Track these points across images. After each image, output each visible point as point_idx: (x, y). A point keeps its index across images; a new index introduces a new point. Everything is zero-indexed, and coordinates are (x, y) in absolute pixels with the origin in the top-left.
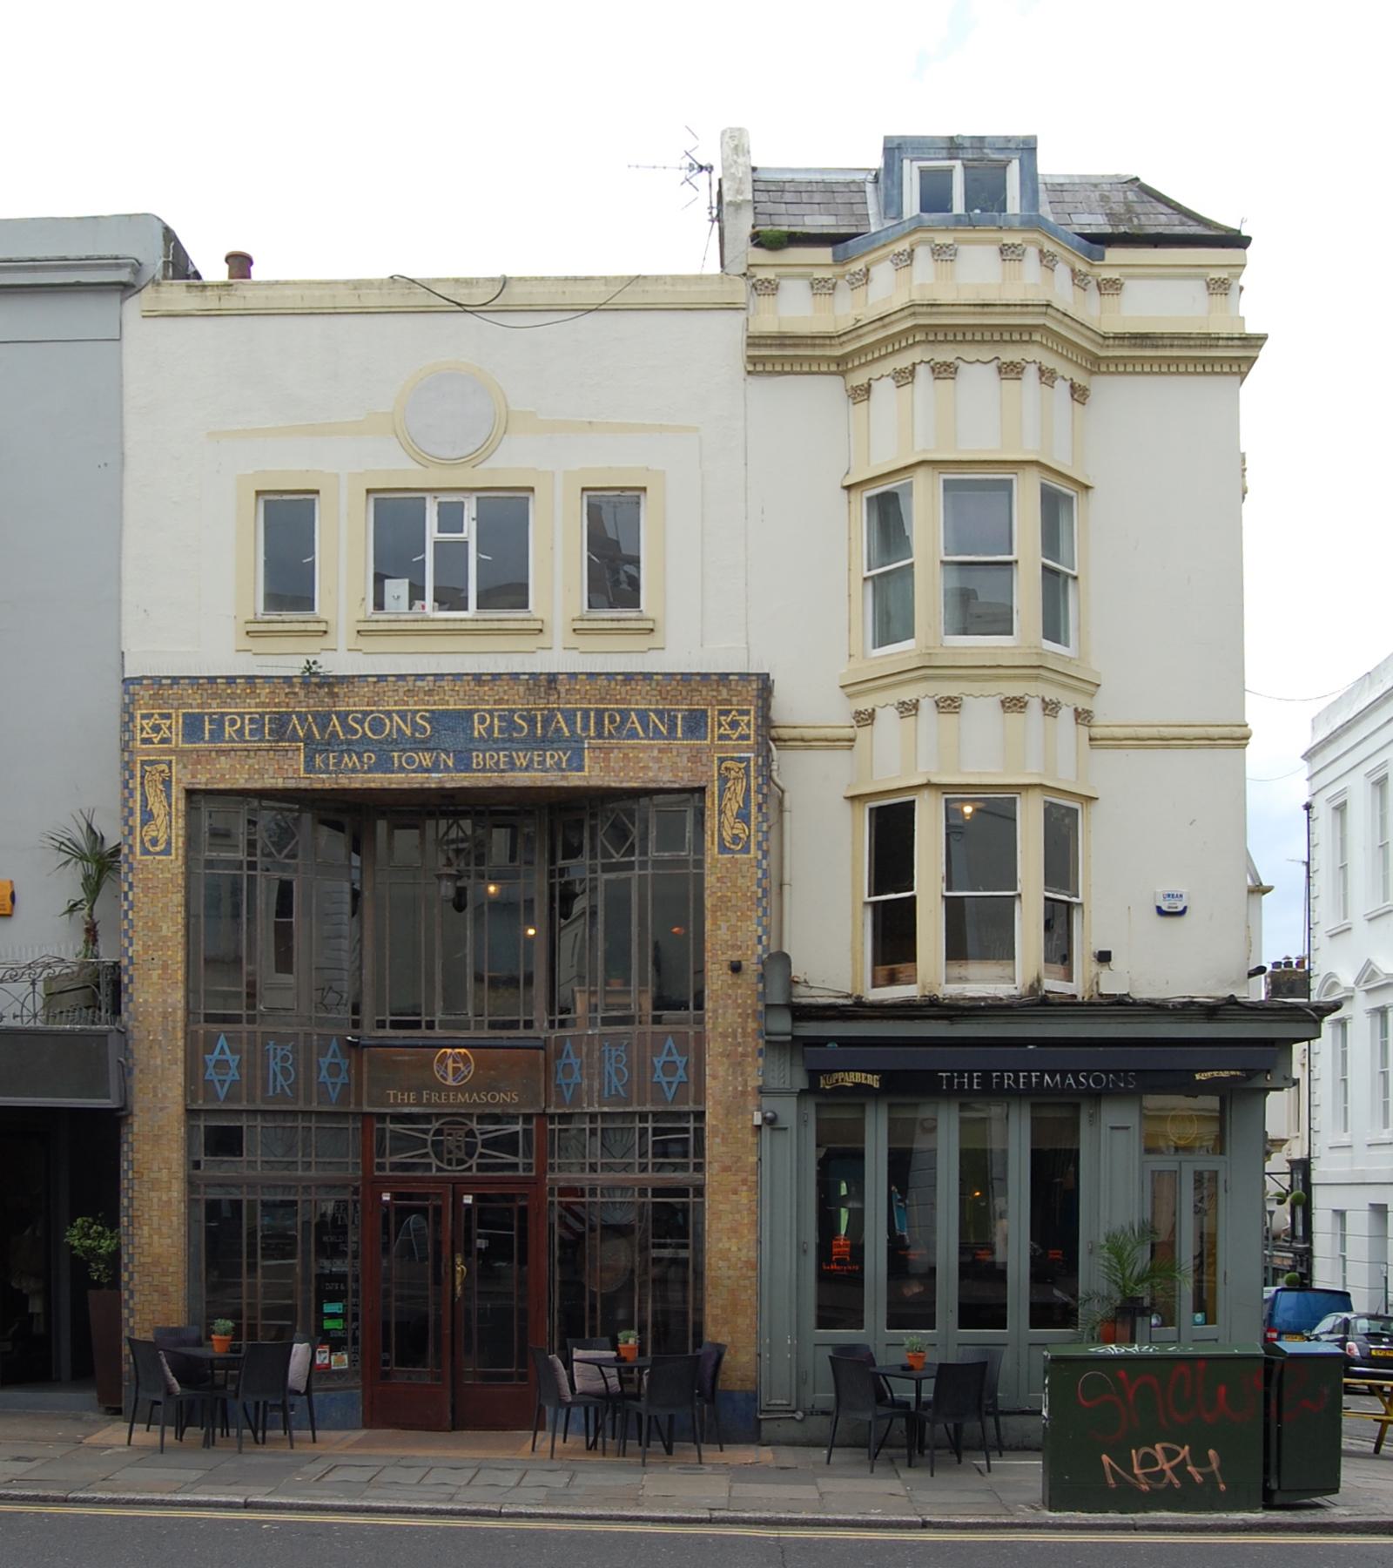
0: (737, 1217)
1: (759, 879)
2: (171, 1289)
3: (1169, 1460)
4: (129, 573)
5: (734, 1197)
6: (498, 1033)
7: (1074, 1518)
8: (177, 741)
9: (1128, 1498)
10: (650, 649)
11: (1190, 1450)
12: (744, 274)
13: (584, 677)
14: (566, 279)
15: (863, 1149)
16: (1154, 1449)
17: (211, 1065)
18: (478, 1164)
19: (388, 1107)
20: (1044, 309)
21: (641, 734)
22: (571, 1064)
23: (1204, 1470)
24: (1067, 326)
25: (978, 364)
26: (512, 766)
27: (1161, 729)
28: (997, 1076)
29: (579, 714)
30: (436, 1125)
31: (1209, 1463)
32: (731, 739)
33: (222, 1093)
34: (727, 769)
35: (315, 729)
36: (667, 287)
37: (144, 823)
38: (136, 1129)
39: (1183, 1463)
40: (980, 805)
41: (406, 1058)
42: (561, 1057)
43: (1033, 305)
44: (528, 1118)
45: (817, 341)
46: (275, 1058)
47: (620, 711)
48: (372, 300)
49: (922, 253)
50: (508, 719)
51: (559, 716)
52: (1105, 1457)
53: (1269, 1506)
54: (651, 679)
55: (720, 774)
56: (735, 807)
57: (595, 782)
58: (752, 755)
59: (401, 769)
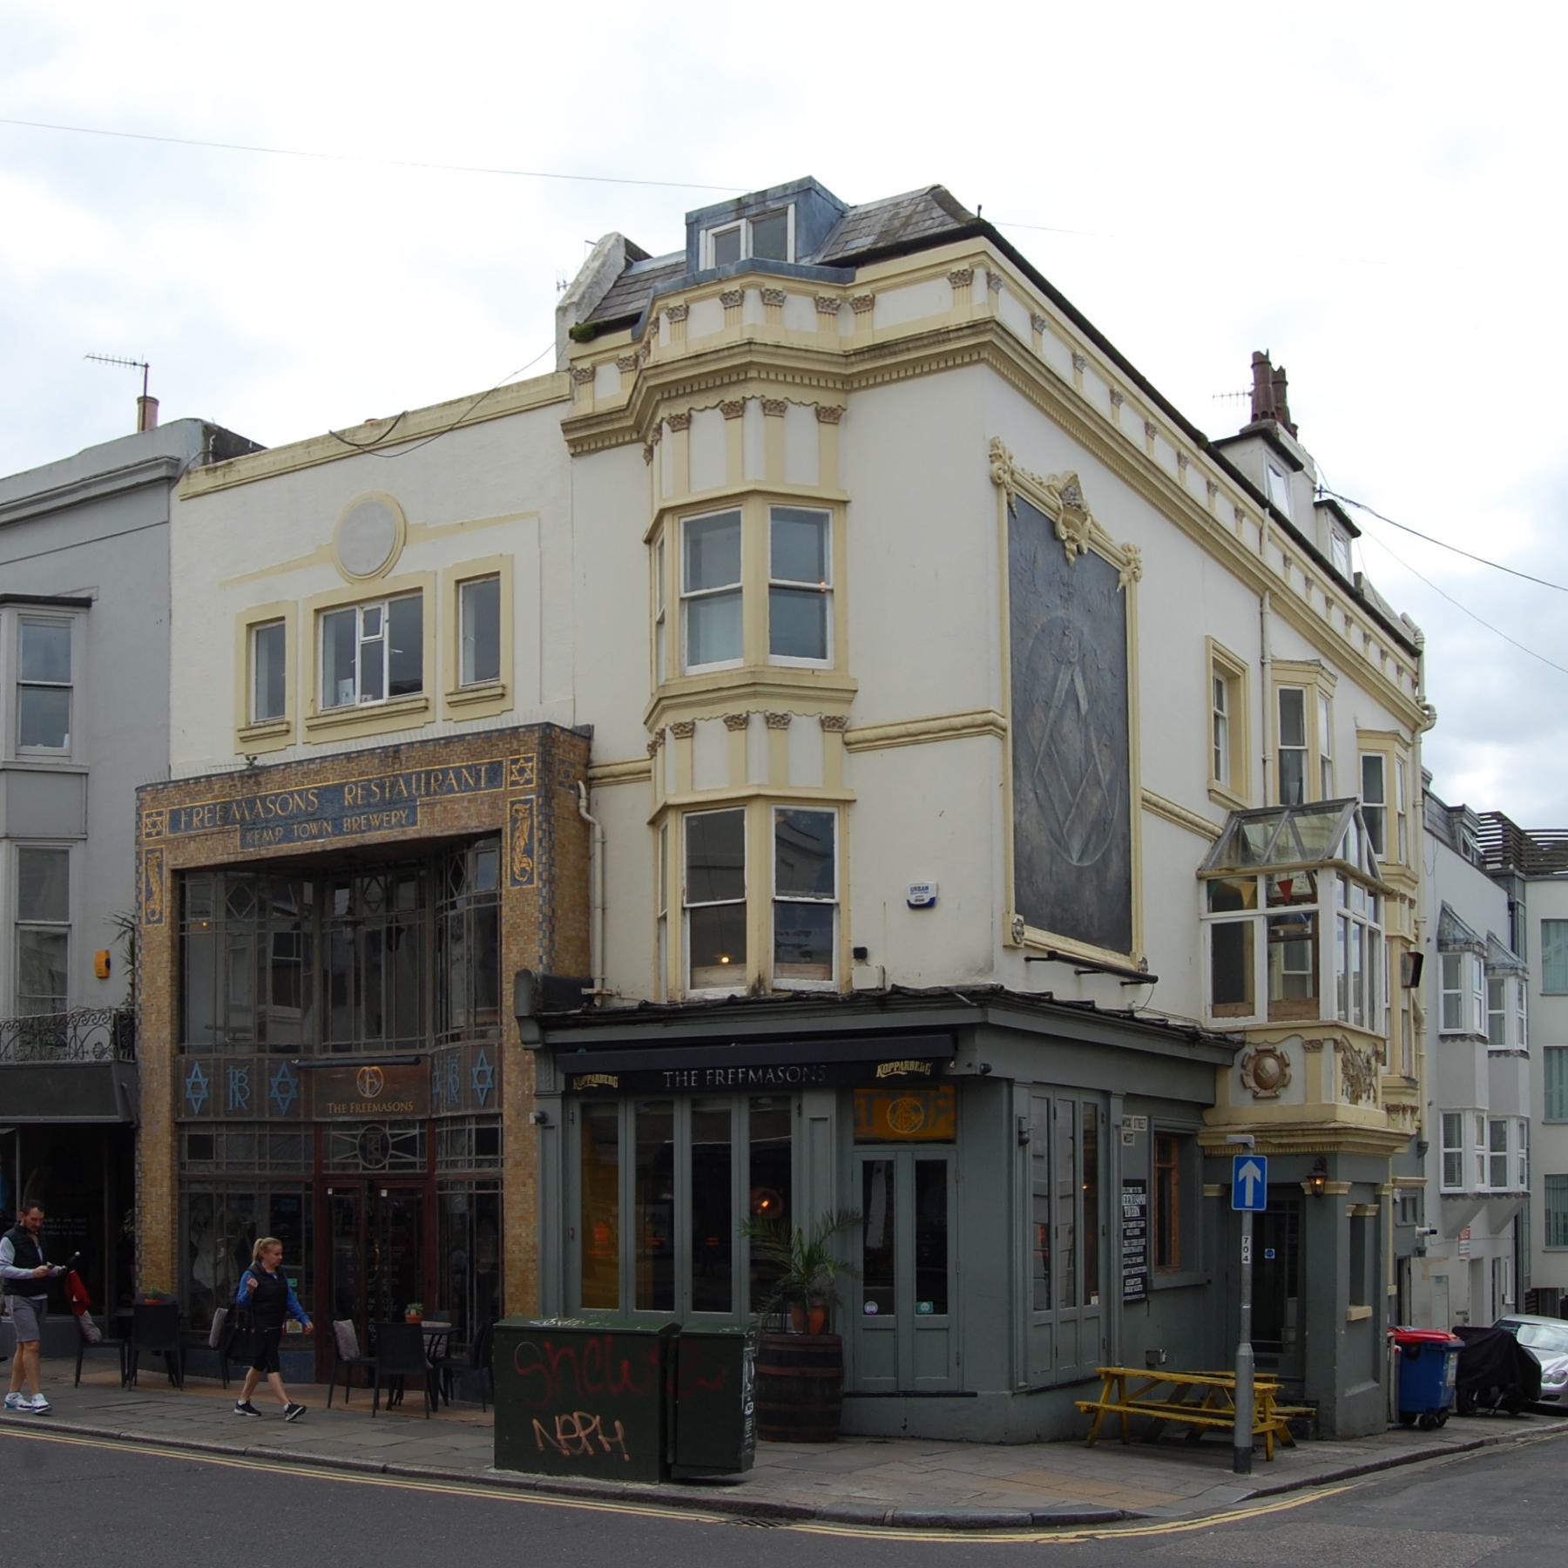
0: (526, 1206)
1: (541, 906)
2: (163, 1264)
3: (584, 1428)
4: (175, 702)
5: (522, 1189)
6: (339, 1055)
7: (531, 1479)
8: (166, 833)
9: (554, 1463)
10: (503, 712)
11: (601, 1420)
12: (569, 369)
13: (418, 745)
14: (445, 405)
15: (789, 1143)
16: (572, 1417)
17: (189, 1086)
18: (390, 1163)
20: (747, 348)
21: (456, 789)
22: (199, 1083)
23: (612, 1440)
24: (784, 356)
25: (708, 411)
26: (370, 828)
27: (953, 719)
28: (710, 1074)
29: (414, 777)
30: (362, 1131)
31: (615, 1435)
32: (519, 784)
33: (196, 1109)
34: (517, 811)
35: (246, 812)
36: (514, 394)
37: (147, 899)
38: (143, 1139)
39: (595, 1431)
41: (340, 1076)
42: (190, 1077)
43: (738, 346)
44: (422, 1123)
45: (614, 416)
46: (234, 1079)
47: (442, 770)
48: (319, 454)
50: (367, 789)
51: (401, 781)
52: (535, 1422)
53: (666, 1476)
54: (464, 740)
55: (511, 816)
56: (523, 844)
57: (425, 834)
59: (299, 839)
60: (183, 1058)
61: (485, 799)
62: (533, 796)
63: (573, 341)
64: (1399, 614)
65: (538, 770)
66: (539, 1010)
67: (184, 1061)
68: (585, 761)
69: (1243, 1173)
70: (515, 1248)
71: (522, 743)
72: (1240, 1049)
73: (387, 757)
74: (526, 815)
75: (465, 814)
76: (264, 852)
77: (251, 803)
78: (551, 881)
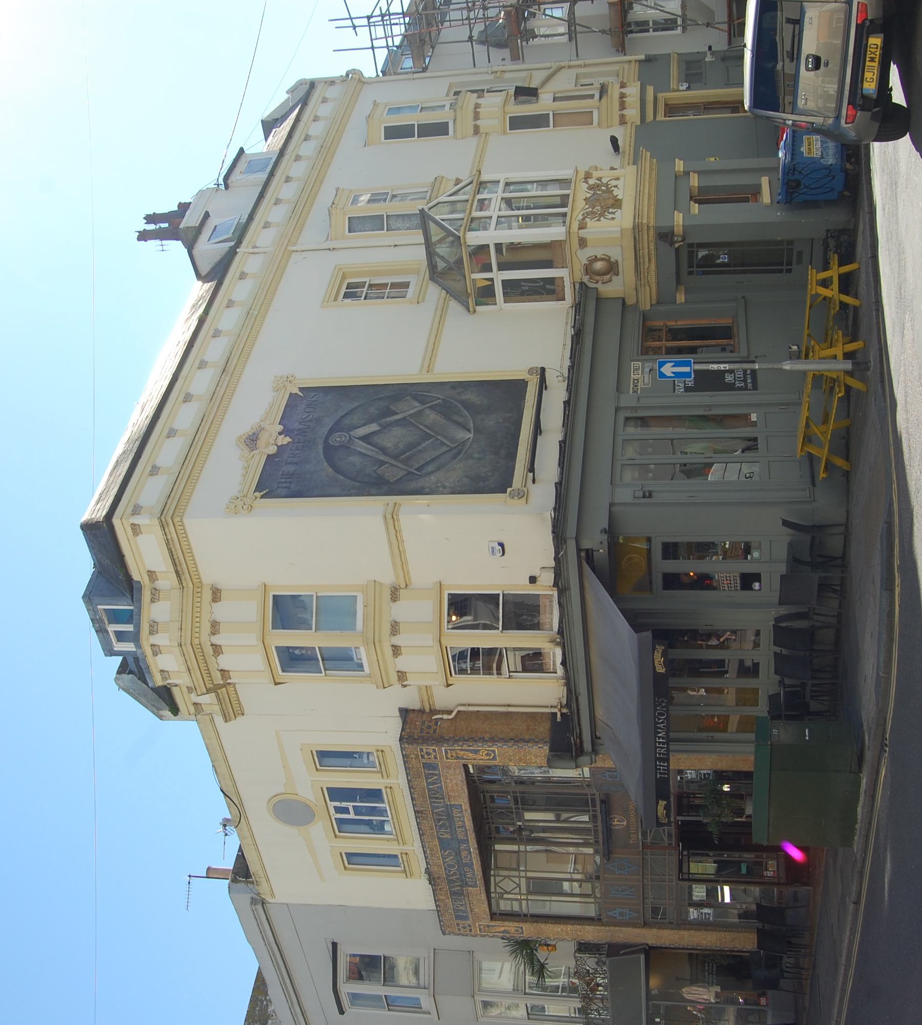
2: (733, 936)
13: (414, 802)
19: (639, 843)
20: (183, 647)
26: (464, 826)
34: (452, 756)
37: (509, 933)
40: (452, 613)
42: (616, 917)
47: (428, 792)
49: (155, 640)
56: (470, 754)
57: (466, 800)
58: (443, 748)
59: (471, 860)
60: (605, 920)
61: (445, 771)
62: (443, 748)
63: (179, 713)
64: (286, 96)
65: (428, 745)
66: (572, 756)
67: (606, 920)
68: (420, 714)
69: (669, 374)
70: (719, 764)
71: (412, 753)
72: (585, 284)
73: (422, 817)
74: (454, 752)
75: (455, 781)
76: (479, 877)
77: (450, 882)
78: (493, 740)
